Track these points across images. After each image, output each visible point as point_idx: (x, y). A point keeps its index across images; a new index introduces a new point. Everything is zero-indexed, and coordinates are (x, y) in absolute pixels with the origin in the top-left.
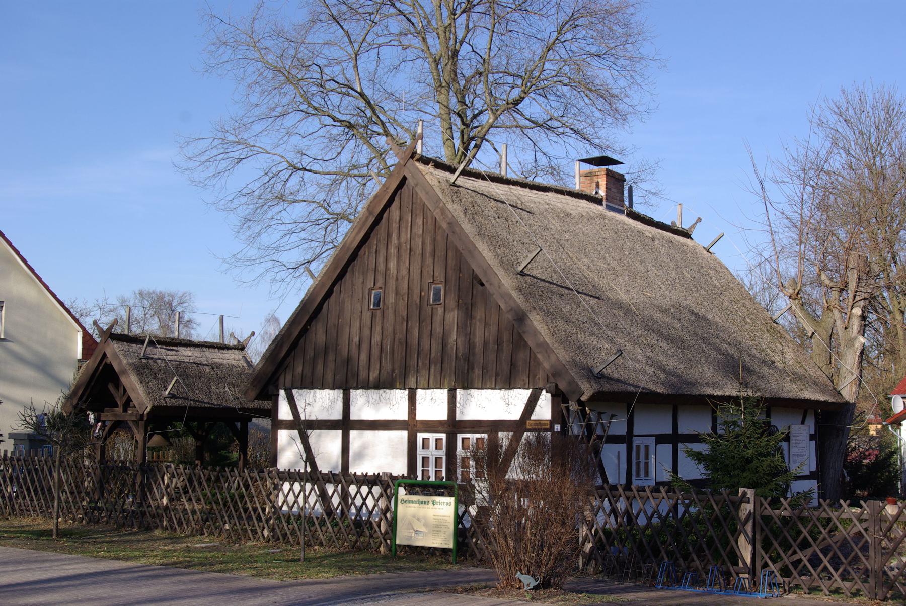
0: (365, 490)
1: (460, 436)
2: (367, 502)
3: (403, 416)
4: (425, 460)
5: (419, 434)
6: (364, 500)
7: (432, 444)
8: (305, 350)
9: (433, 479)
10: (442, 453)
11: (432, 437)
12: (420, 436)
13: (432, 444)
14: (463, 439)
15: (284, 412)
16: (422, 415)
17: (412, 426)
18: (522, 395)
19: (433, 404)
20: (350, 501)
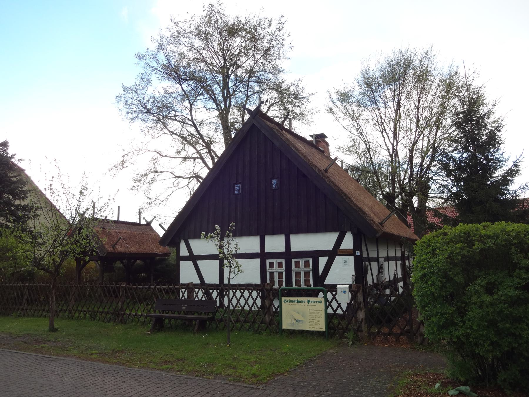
0: (246, 294)
1: (293, 261)
2: (198, 295)
3: (257, 250)
4: (272, 275)
5: (267, 260)
6: (238, 301)
7: (276, 265)
8: (187, 224)
9: (303, 286)
10: (283, 269)
11: (275, 261)
12: (268, 262)
13: (276, 265)
14: (270, 263)
15: (184, 252)
16: (268, 249)
17: (263, 256)
18: (333, 237)
19: (275, 243)
20: (195, 295)
